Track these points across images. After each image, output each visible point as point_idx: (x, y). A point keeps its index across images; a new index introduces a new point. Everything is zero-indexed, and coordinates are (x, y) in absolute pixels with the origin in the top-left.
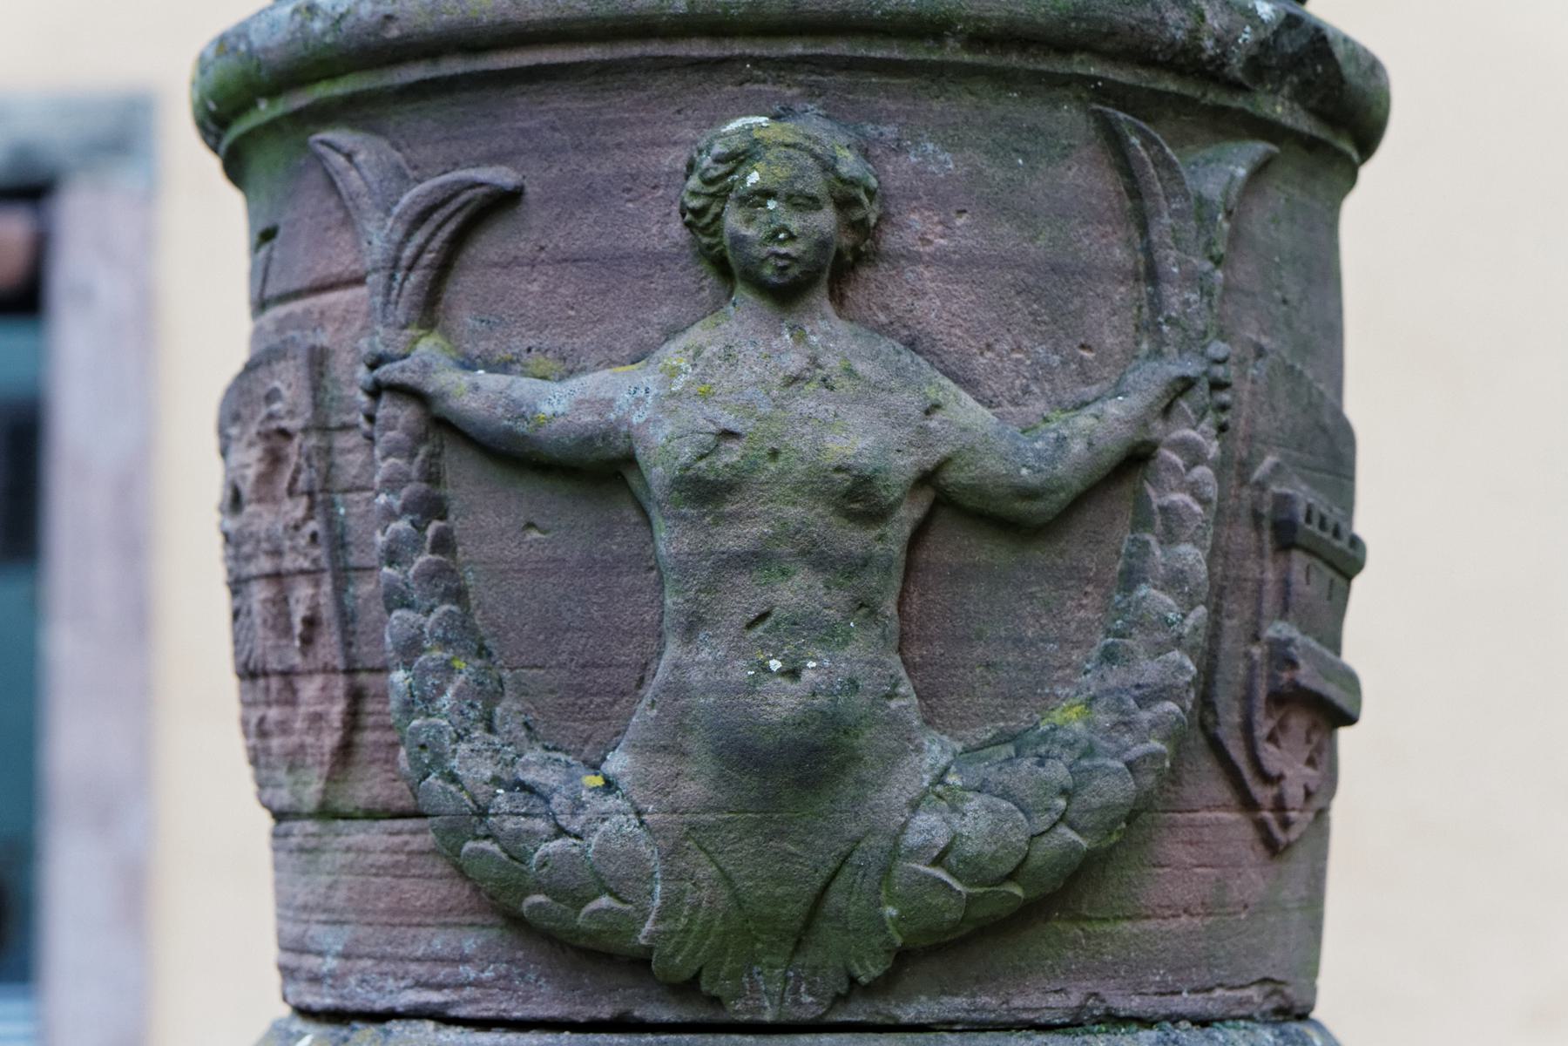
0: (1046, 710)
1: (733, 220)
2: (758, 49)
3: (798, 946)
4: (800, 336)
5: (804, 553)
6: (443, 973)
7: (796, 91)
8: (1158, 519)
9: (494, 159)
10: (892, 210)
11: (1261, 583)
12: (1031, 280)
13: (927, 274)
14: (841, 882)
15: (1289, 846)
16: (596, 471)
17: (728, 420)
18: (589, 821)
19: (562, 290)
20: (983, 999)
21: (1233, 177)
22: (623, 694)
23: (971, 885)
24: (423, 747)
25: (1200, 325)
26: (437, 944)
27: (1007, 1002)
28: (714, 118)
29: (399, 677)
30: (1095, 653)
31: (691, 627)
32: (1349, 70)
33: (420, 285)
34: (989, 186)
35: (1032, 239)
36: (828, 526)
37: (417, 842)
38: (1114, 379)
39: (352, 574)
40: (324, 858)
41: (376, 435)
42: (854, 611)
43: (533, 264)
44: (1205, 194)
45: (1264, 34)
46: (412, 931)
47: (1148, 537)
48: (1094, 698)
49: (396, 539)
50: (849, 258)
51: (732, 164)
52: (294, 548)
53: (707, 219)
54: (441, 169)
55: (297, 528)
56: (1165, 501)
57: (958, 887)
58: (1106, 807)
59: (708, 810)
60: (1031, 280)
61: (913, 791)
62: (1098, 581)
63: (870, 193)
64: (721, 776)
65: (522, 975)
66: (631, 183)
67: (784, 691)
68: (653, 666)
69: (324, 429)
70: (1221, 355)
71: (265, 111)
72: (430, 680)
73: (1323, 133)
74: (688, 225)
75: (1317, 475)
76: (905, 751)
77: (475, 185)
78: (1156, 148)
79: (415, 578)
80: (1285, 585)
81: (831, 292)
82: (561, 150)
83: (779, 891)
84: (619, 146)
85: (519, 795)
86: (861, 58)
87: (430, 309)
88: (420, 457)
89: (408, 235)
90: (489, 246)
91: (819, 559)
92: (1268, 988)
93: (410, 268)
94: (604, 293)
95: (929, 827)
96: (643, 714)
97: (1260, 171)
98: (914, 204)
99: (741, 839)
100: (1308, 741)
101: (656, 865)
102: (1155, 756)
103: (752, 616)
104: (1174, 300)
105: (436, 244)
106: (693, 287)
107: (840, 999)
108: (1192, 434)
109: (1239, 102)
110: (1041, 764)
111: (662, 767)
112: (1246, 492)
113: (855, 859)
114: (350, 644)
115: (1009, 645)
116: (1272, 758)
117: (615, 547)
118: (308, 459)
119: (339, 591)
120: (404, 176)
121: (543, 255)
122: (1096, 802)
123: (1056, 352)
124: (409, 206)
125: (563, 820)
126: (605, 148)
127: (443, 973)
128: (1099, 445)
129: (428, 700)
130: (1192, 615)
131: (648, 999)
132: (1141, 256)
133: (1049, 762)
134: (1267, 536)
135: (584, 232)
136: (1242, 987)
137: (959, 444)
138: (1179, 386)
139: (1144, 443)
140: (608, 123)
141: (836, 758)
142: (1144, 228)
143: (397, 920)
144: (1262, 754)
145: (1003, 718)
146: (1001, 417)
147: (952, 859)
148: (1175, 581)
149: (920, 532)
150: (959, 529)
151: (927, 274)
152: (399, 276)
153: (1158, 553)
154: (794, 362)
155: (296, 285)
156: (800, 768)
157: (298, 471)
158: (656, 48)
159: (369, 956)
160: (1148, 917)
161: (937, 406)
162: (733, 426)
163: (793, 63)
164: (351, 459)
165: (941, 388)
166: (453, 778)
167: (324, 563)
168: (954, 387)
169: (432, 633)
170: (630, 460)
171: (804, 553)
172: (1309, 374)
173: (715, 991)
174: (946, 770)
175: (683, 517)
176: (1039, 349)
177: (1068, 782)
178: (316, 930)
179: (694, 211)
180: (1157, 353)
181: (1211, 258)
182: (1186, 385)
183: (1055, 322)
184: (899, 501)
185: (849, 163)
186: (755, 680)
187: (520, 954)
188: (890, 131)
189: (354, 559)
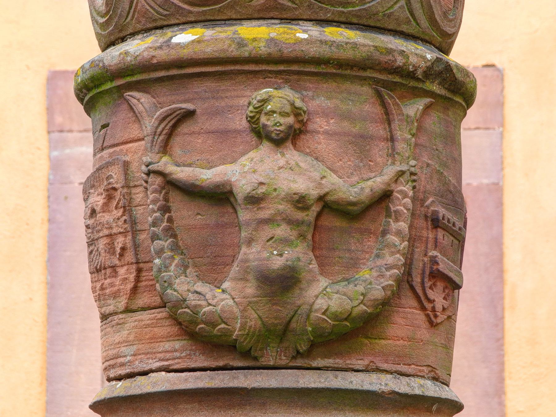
0: (357, 272)
1: (263, 119)
2: (312, 69)
3: (281, 341)
4: (283, 155)
5: (284, 219)
6: (168, 355)
7: (281, 81)
8: (393, 214)
9: (185, 101)
10: (311, 117)
11: (428, 238)
12: (354, 140)
13: (322, 137)
14: (294, 319)
15: (437, 324)
16: (220, 197)
17: (262, 180)
18: (218, 301)
19: (208, 142)
20: (337, 361)
21: (418, 109)
22: (228, 265)
23: (334, 321)
24: (165, 282)
25: (407, 155)
26: (166, 346)
27: (345, 362)
28: (256, 89)
29: (157, 261)
30: (373, 255)
31: (250, 242)
32: (459, 76)
33: (163, 140)
34: (341, 110)
35: (354, 127)
36: (291, 211)
37: (159, 316)
38: (380, 171)
39: (138, 232)
40: (126, 325)
41: (148, 187)
42: (299, 237)
43: (199, 133)
44: (409, 114)
45: (429, 64)
46: (158, 344)
47: (390, 220)
48: (372, 268)
49: (156, 219)
50: (298, 132)
51: (263, 103)
52: (117, 226)
53: (255, 119)
54: (169, 104)
55: (118, 219)
56: (395, 209)
57: (330, 321)
58: (375, 300)
59: (255, 297)
60: (354, 140)
61: (316, 292)
62: (375, 234)
63: (305, 112)
64: (259, 286)
65: (194, 354)
66: (231, 109)
67: (278, 260)
68: (237, 256)
69: (128, 187)
70: (413, 164)
71: (108, 86)
72: (167, 261)
73: (449, 95)
74: (249, 121)
75: (448, 206)
76: (314, 280)
77: (181, 109)
78: (393, 100)
79: (162, 230)
80: (436, 240)
81: (292, 142)
82: (208, 98)
83: (276, 322)
84: (226, 97)
85: (196, 295)
86: (96, 94)
87: (165, 149)
88: (163, 193)
89: (159, 124)
90: (184, 128)
91: (290, 222)
92: (430, 369)
93: (160, 135)
94: (222, 142)
95: (321, 303)
96: (235, 269)
97: (428, 108)
98: (318, 116)
99: (264, 306)
100: (444, 291)
101: (238, 314)
102: (391, 286)
103: (268, 238)
104: (399, 147)
105: (168, 127)
106: (250, 141)
107: (294, 358)
108: (404, 188)
109: (420, 85)
110: (356, 286)
111: (240, 285)
112: (422, 209)
113: (299, 312)
114: (138, 254)
115: (346, 252)
116: (431, 294)
117: (225, 219)
118: (124, 196)
119: (134, 238)
120: (156, 106)
121: (202, 131)
122: (372, 298)
123: (361, 162)
124: (160, 115)
125: (210, 301)
126: (222, 98)
127: (168, 355)
128: (374, 191)
129: (166, 267)
130: (403, 244)
131: (234, 359)
132: (389, 133)
133: (358, 286)
134: (429, 223)
135: (216, 124)
136: (420, 366)
137: (331, 188)
138: (400, 173)
139: (389, 191)
140: (223, 90)
141: (293, 281)
142: (389, 124)
143: (152, 341)
144: (427, 292)
145: (344, 273)
146: (344, 181)
147: (328, 313)
148: (399, 233)
149: (319, 215)
150: (332, 220)
151: (322, 137)
152: (156, 137)
153: (393, 225)
154: (282, 162)
155: (116, 142)
156: (281, 284)
157: (119, 200)
158: (238, 67)
159: (143, 354)
160: (390, 339)
161: (324, 177)
162: (263, 181)
163: (280, 72)
164: (138, 196)
165: (326, 172)
166: (175, 291)
167: (129, 229)
168: (329, 171)
169: (167, 247)
170: (231, 192)
171: (284, 219)
172: (445, 173)
173: (256, 355)
174: (326, 287)
175: (248, 208)
176: (356, 161)
177: (364, 292)
178: (123, 349)
179: (250, 117)
180: (393, 163)
181: (411, 134)
182: (402, 173)
183: (361, 153)
184: (313, 204)
185: (298, 103)
186: (269, 257)
187: (194, 348)
188: (310, 93)
189: (139, 227)
